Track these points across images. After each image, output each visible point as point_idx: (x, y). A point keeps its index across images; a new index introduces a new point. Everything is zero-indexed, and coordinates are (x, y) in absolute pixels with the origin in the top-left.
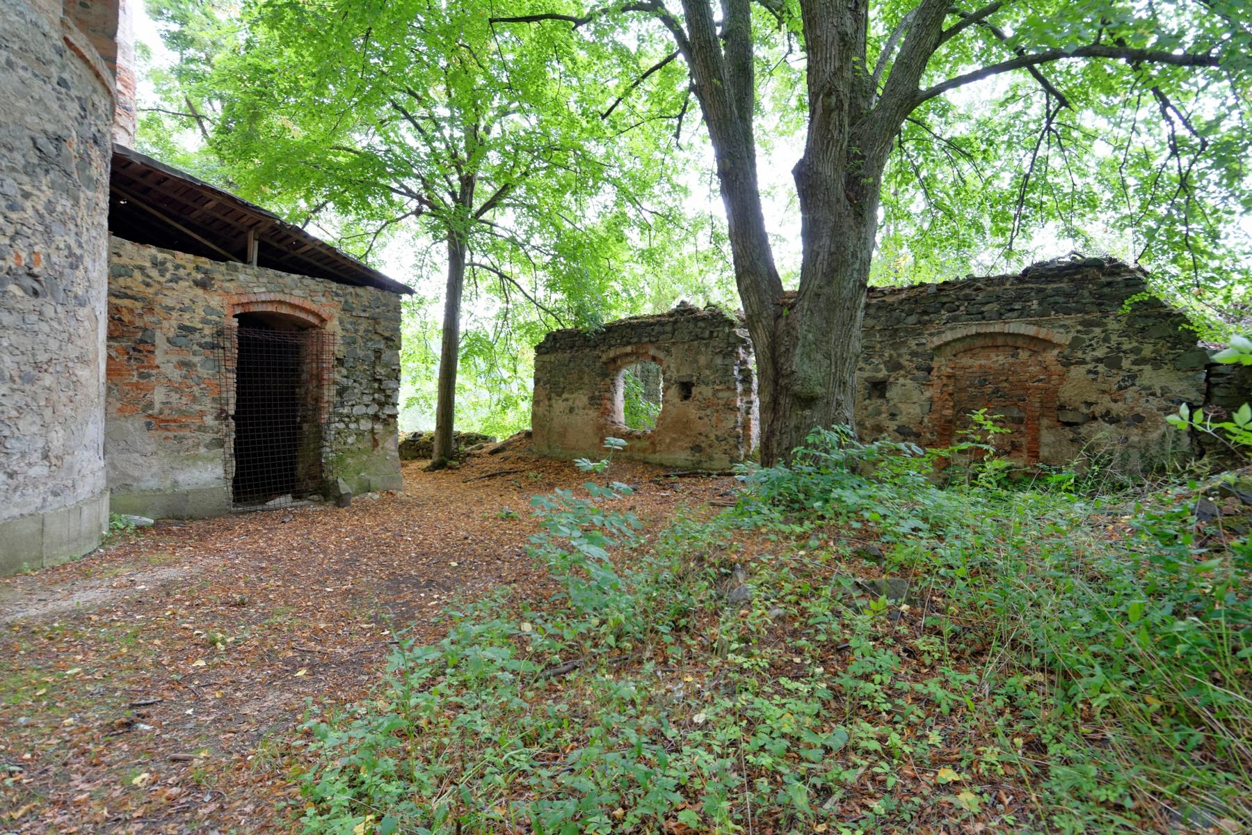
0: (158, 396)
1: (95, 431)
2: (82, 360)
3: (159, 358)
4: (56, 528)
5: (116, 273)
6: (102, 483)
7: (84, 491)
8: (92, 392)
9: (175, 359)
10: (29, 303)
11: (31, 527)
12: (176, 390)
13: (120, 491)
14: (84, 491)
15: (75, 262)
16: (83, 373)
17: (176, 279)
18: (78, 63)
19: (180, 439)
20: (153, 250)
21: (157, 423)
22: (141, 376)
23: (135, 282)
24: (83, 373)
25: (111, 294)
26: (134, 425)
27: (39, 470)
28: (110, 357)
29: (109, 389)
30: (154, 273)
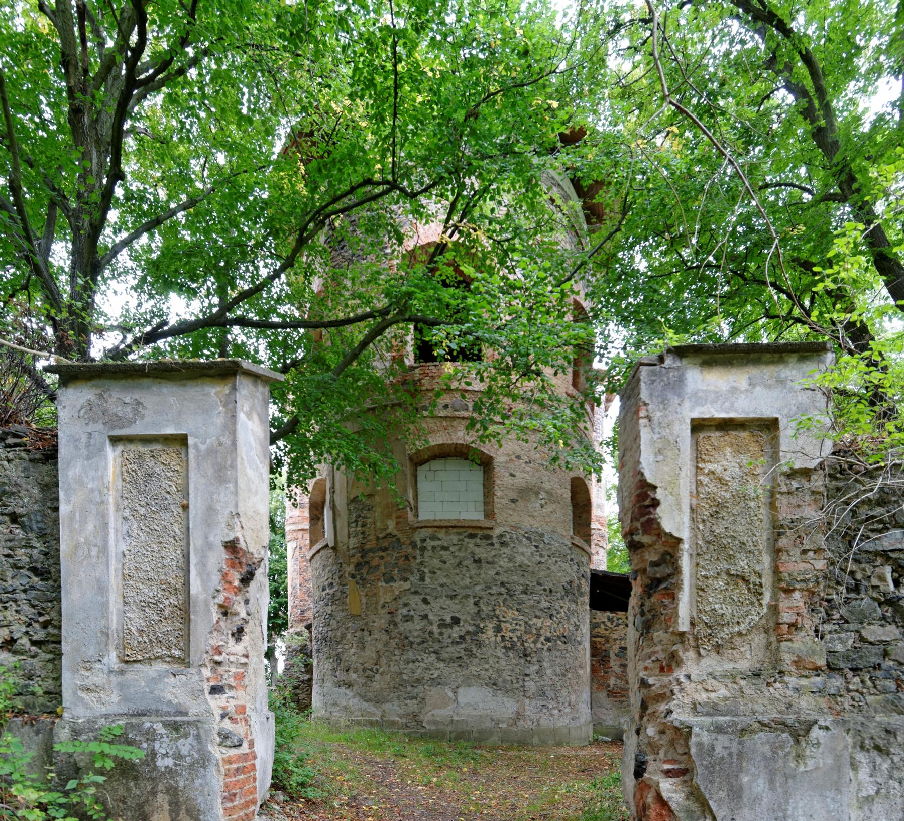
0: (612, 681)
1: (586, 696)
2: (581, 667)
3: (612, 663)
4: (573, 732)
5: (594, 626)
6: (589, 718)
7: (582, 720)
8: (584, 680)
9: (618, 663)
10: (563, 646)
11: (566, 731)
12: (619, 678)
13: (597, 724)
14: (582, 720)
15: (577, 627)
16: (581, 672)
17: (618, 625)
18: (577, 549)
19: (621, 702)
20: (608, 613)
21: (612, 694)
22: (606, 672)
23: (601, 630)
24: (581, 672)
25: (592, 636)
26: (602, 695)
27: (568, 710)
28: (592, 665)
29: (592, 680)
30: (609, 624)
